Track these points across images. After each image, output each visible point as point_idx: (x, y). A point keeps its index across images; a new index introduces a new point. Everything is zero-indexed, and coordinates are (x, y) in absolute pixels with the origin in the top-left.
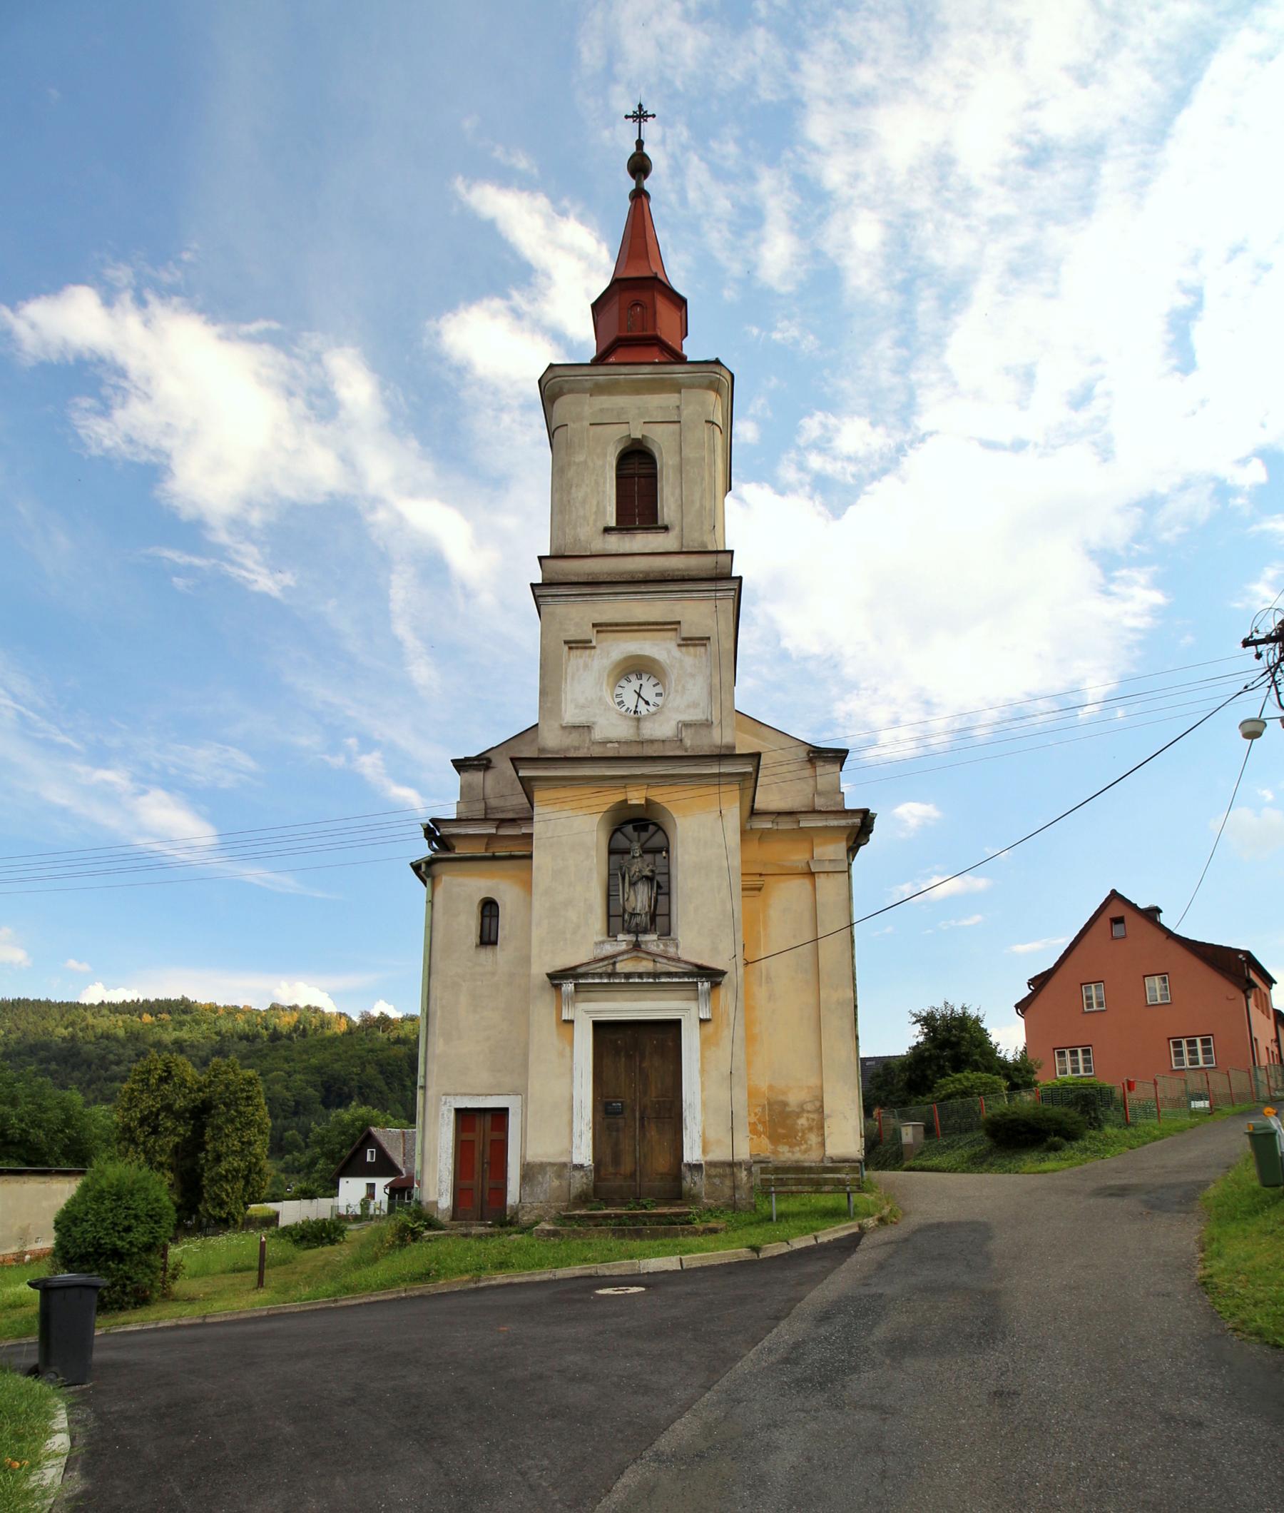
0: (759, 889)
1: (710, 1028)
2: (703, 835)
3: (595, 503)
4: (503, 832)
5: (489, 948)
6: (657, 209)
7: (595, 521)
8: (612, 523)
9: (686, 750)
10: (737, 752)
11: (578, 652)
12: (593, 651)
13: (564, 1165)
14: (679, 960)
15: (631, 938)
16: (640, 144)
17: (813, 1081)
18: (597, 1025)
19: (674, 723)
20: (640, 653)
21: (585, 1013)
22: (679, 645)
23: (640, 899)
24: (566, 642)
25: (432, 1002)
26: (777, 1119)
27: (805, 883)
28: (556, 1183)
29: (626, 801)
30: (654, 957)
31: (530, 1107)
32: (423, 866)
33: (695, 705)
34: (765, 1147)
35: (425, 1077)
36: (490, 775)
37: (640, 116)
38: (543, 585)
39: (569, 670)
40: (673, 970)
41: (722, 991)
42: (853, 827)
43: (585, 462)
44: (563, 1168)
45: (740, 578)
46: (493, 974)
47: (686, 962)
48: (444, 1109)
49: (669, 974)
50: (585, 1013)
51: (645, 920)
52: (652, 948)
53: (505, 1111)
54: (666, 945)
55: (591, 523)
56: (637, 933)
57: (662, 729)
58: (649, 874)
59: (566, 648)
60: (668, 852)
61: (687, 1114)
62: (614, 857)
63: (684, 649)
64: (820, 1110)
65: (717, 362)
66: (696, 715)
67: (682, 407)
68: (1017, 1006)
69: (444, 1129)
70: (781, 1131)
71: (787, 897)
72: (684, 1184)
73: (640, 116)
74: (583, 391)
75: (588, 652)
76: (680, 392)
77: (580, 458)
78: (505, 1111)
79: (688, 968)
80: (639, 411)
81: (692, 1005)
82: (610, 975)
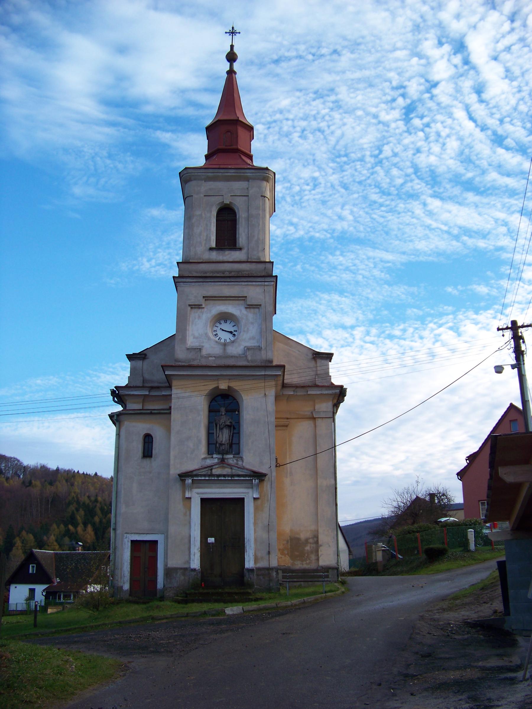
0: (287, 426)
1: (259, 502)
2: (257, 404)
3: (205, 234)
4: (154, 393)
5: (148, 459)
7: (205, 244)
8: (214, 245)
9: (248, 361)
10: (275, 363)
11: (196, 310)
12: (203, 310)
13: (185, 569)
14: (243, 468)
15: (220, 456)
16: (232, 47)
17: (313, 527)
19: (242, 347)
20: (227, 311)
21: (196, 495)
22: (246, 308)
23: (224, 436)
24: (189, 305)
25: (119, 486)
26: (295, 545)
28: (182, 578)
29: (218, 387)
30: (231, 466)
31: (169, 541)
32: (115, 416)
33: (253, 338)
34: (287, 562)
35: (115, 524)
36: (146, 362)
37: (233, 33)
38: (180, 277)
39: (191, 319)
40: (241, 473)
41: (265, 483)
42: (335, 394)
43: (201, 215)
44: (186, 570)
45: (276, 276)
46: (150, 472)
47: (247, 469)
48: (126, 540)
49: (239, 476)
50: (196, 495)
51: (226, 447)
52: (231, 462)
53: (156, 542)
54: (237, 460)
55: (203, 244)
57: (236, 350)
58: (229, 424)
59: (189, 308)
60: (239, 411)
61: (247, 544)
63: (248, 310)
64: (317, 542)
67: (249, 189)
69: (126, 550)
70: (297, 553)
71: (302, 430)
72: (245, 579)
74: (202, 180)
75: (200, 310)
76: (249, 181)
77: (198, 213)
78: (156, 542)
79: (248, 473)
80: (229, 191)
81: (250, 491)
82: (209, 476)
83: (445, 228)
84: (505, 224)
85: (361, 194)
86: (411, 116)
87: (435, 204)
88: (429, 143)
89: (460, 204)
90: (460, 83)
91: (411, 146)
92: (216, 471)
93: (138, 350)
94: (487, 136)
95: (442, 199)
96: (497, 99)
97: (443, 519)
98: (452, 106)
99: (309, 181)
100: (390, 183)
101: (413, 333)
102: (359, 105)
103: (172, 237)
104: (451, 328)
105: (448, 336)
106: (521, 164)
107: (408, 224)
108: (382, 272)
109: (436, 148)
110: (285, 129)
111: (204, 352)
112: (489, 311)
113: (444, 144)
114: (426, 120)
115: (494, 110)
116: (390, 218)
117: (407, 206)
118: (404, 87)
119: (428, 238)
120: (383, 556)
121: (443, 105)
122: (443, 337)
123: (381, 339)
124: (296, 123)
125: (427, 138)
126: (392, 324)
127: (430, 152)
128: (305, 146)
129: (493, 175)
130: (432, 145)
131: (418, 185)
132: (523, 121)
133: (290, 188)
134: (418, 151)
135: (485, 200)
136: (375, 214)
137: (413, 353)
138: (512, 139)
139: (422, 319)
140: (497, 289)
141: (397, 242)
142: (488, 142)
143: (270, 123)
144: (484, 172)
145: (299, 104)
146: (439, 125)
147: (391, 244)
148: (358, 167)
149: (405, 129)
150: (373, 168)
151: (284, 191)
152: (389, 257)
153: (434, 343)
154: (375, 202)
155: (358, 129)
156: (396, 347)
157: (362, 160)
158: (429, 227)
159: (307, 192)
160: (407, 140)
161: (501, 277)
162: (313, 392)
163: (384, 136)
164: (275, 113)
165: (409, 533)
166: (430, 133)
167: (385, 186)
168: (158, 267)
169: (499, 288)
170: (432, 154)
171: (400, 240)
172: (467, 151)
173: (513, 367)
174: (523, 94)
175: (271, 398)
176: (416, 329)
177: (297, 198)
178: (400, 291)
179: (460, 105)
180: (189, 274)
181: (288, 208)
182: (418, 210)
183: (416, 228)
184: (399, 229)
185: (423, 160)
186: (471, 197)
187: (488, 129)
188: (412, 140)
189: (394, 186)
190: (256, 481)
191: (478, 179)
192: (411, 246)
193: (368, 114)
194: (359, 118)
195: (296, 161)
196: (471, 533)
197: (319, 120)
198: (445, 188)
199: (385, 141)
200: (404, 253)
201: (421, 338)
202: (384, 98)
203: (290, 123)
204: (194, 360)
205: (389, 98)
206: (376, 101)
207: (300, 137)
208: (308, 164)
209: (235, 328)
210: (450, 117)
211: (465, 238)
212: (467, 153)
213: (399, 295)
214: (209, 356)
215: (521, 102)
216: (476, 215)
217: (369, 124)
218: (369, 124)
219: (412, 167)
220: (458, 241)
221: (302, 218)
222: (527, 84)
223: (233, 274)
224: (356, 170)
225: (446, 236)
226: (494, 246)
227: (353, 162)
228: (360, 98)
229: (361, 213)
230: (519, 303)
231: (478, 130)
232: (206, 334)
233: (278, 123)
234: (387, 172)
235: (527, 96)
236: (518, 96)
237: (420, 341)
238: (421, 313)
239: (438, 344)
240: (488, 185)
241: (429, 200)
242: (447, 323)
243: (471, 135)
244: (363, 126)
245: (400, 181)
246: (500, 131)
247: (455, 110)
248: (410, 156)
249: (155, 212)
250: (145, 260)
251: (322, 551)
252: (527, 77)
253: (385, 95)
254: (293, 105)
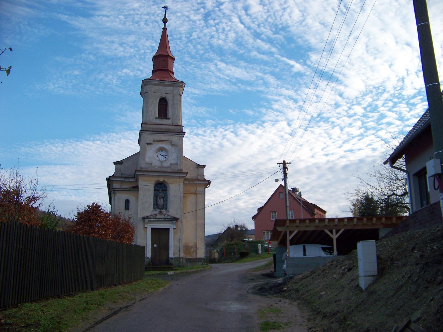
1: (176, 230)
2: (175, 189)
6: (168, 31)
8: (157, 116)
9: (172, 169)
10: (183, 171)
14: (169, 216)
17: (195, 241)
18: (152, 229)
19: (169, 163)
21: (149, 227)
23: (161, 202)
26: (187, 248)
27: (195, 195)
29: (159, 180)
30: (164, 215)
33: (174, 159)
36: (122, 165)
56: (161, 209)
57: (166, 164)
62: (155, 192)
64: (196, 247)
65: (182, 82)
66: (173, 162)
68: (253, 217)
73: (166, 8)
79: (172, 218)
80: (165, 91)
81: (172, 225)
83: (228, 78)
84: (262, 79)
85: (179, 57)
86: (209, 18)
87: (222, 65)
88: (219, 33)
89: (237, 66)
90: (236, 5)
91: (209, 34)
92: (158, 217)
93: (119, 160)
94: (251, 33)
95: (226, 63)
96: (256, 15)
97: (246, 239)
98: (231, 16)
99: (150, 48)
100: (196, 52)
101: (210, 133)
102: (179, 10)
103: (68, 72)
104: (232, 132)
105: (230, 136)
106: (270, 49)
107: (207, 75)
108: (192, 99)
109: (223, 37)
110: (136, 19)
111: (153, 165)
112: (254, 124)
113: (227, 35)
114: (216, 21)
115: (255, 20)
116: (196, 71)
117: (206, 65)
118: (204, 4)
119: (219, 83)
120: (218, 256)
121: (226, 15)
122: (228, 136)
123: (191, 135)
124: (142, 17)
125: (217, 30)
126: (198, 128)
127: (219, 39)
128: (147, 29)
129: (255, 53)
130: (220, 34)
131: (212, 55)
132: (270, 27)
133: (138, 51)
134: (212, 37)
135: (251, 66)
136: (188, 68)
137: (210, 144)
138: (265, 35)
139: (215, 126)
140: (258, 112)
141: (201, 84)
142: (252, 36)
143: (127, 15)
144: (250, 51)
145: (144, 7)
146: (224, 24)
147: (197, 84)
148: (178, 42)
149: (204, 24)
150: (186, 44)
151: (135, 52)
152: (196, 91)
153: (223, 139)
154: (188, 62)
155: (178, 23)
156: (200, 140)
157: (180, 39)
158: (219, 77)
159: (148, 54)
160: (206, 31)
161: (261, 106)
162: (196, 181)
163: (193, 28)
164: (130, 10)
165: (230, 245)
166: (219, 28)
167: (193, 53)
168: (59, 89)
169: (260, 112)
170: (220, 39)
171: (202, 83)
172: (240, 39)
173: (282, 180)
174: (270, 13)
175: (182, 184)
176: (212, 131)
177: (142, 56)
178: (202, 110)
179: (236, 16)
180: (146, 130)
181: (137, 61)
182: (213, 68)
183: (211, 77)
184: (202, 77)
185: (215, 42)
186: (242, 63)
187: (252, 29)
188: (209, 31)
189: (199, 54)
190: (175, 221)
191: (246, 54)
192: (209, 86)
193: (183, 15)
194: (179, 17)
195: (142, 37)
196: (259, 245)
197: (156, 16)
198: (228, 57)
199: (193, 31)
200: (204, 90)
201: (215, 136)
202: (193, 8)
203: (139, 16)
204: (148, 168)
205: (196, 8)
206: (188, 9)
207: (145, 24)
208: (149, 39)
209: (166, 154)
210: (230, 21)
211: (240, 85)
212: (240, 41)
213: (202, 112)
214: (155, 167)
215: (269, 18)
216: (245, 73)
217: (184, 21)
218: (184, 21)
219: (209, 45)
220: (235, 86)
221: (145, 67)
222: (272, 9)
223: (166, 130)
224: (177, 44)
225: (229, 83)
226: (256, 90)
227: (175, 39)
228: (179, 6)
229: (180, 67)
230: (271, 121)
231: (246, 29)
232: (154, 157)
233: (132, 16)
234: (195, 47)
235: (273, 15)
236: (268, 14)
237: (214, 138)
238: (214, 123)
239: (225, 140)
240: (252, 58)
241: (219, 63)
242: (229, 129)
243: (242, 31)
244: (181, 22)
245: (202, 52)
246: (258, 31)
247: (233, 18)
248: (208, 39)
249: (58, 58)
250: (51, 84)
251: (198, 251)
252: (272, 5)
253: (193, 6)
254: (140, 7)
